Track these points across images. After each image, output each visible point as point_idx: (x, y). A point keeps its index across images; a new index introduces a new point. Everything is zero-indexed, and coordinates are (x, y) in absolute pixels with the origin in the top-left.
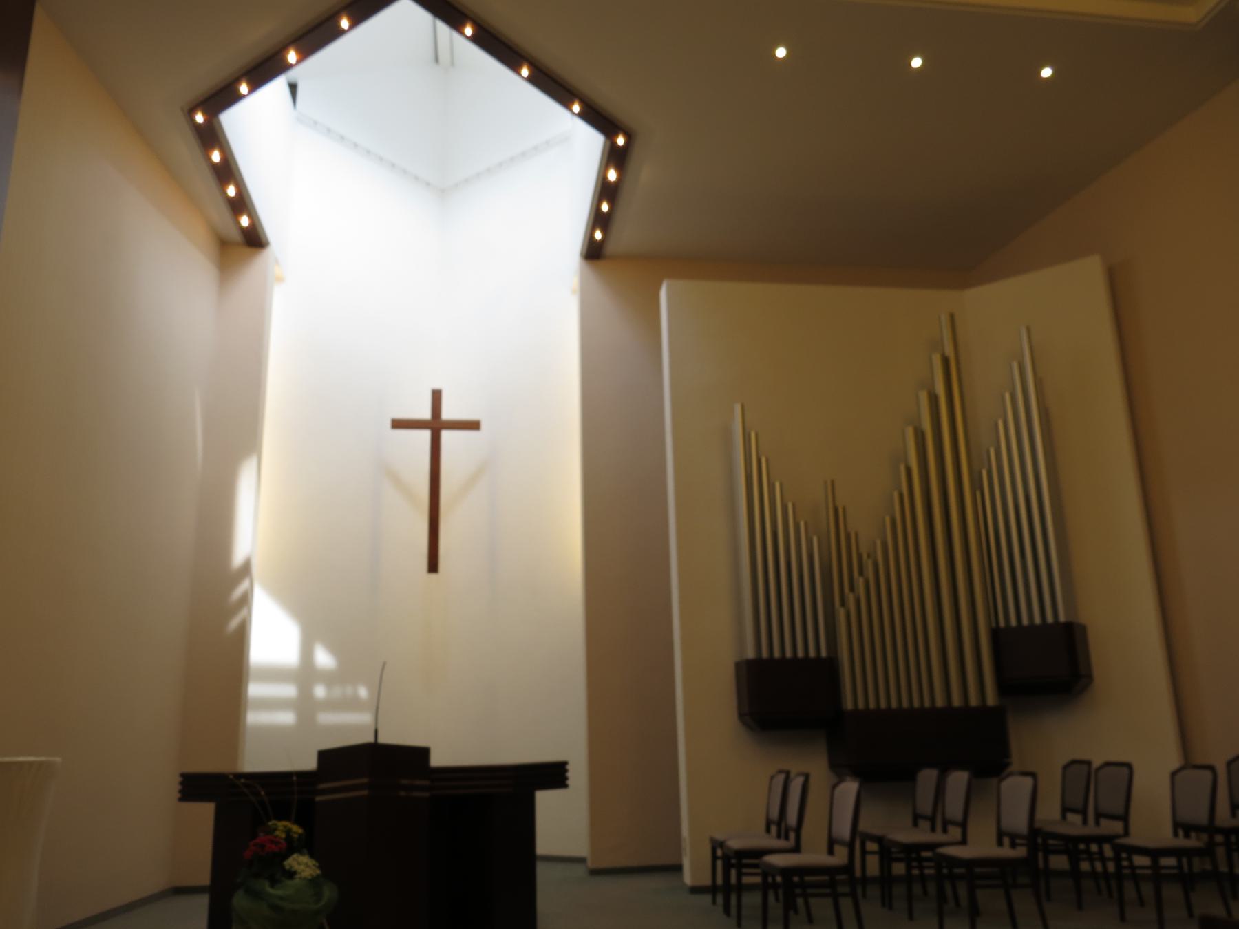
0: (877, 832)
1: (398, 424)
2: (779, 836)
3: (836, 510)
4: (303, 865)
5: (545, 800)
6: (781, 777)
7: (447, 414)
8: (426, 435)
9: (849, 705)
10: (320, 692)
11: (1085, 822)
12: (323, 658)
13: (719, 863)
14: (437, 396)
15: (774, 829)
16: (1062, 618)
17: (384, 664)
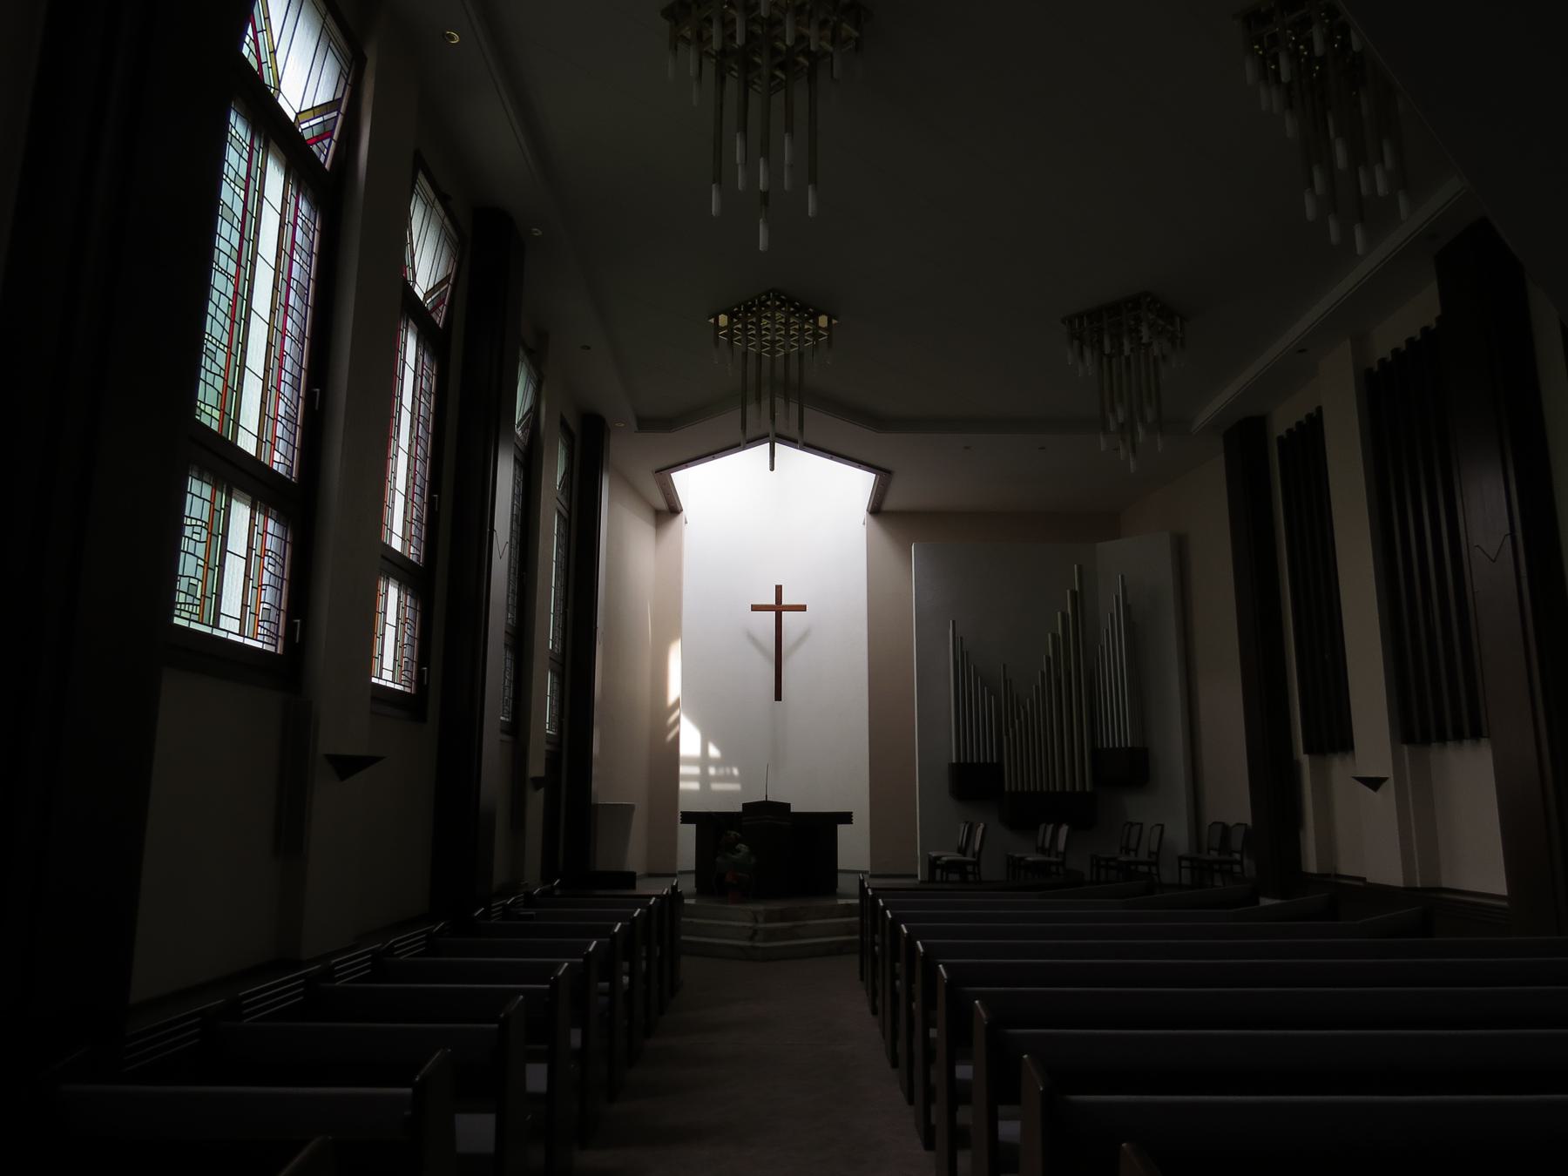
1: (755, 608)
4: (743, 847)
5: (841, 828)
8: (773, 614)
10: (712, 771)
12: (714, 752)
14: (779, 589)
15: (1124, 851)
17: (772, 469)
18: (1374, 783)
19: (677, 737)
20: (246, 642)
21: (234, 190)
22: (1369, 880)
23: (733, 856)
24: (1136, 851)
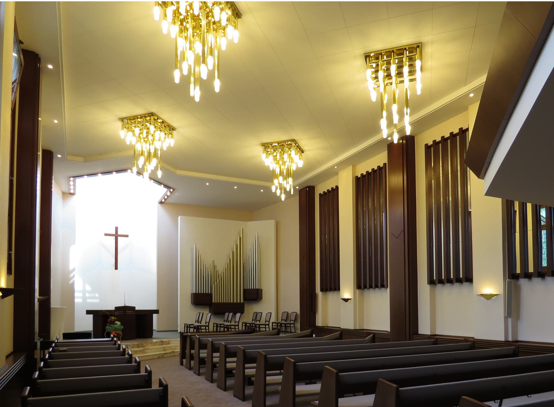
0: (216, 323)
2: (197, 323)
3: (214, 266)
4: (119, 323)
6: (199, 313)
7: (120, 233)
9: (214, 302)
10: (87, 295)
11: (255, 321)
12: (88, 288)
13: (186, 328)
14: (117, 229)
15: (197, 322)
16: (257, 288)
18: (346, 300)
19: (73, 283)
20: (461, 241)
21: (191, 8)
22: (341, 328)
23: (114, 326)
24: (260, 321)
